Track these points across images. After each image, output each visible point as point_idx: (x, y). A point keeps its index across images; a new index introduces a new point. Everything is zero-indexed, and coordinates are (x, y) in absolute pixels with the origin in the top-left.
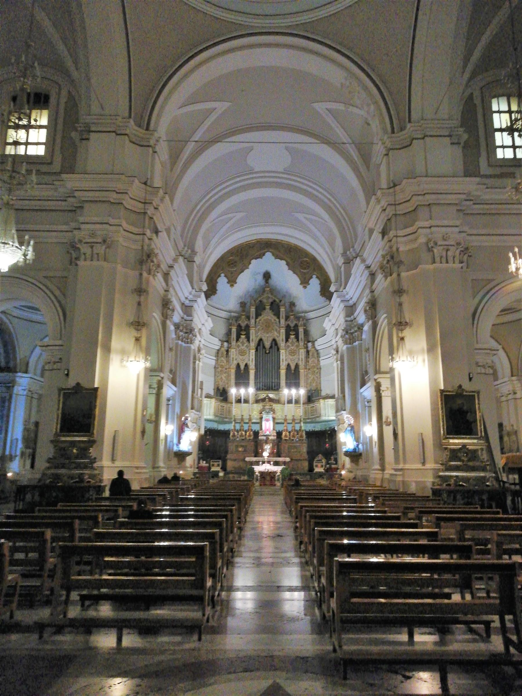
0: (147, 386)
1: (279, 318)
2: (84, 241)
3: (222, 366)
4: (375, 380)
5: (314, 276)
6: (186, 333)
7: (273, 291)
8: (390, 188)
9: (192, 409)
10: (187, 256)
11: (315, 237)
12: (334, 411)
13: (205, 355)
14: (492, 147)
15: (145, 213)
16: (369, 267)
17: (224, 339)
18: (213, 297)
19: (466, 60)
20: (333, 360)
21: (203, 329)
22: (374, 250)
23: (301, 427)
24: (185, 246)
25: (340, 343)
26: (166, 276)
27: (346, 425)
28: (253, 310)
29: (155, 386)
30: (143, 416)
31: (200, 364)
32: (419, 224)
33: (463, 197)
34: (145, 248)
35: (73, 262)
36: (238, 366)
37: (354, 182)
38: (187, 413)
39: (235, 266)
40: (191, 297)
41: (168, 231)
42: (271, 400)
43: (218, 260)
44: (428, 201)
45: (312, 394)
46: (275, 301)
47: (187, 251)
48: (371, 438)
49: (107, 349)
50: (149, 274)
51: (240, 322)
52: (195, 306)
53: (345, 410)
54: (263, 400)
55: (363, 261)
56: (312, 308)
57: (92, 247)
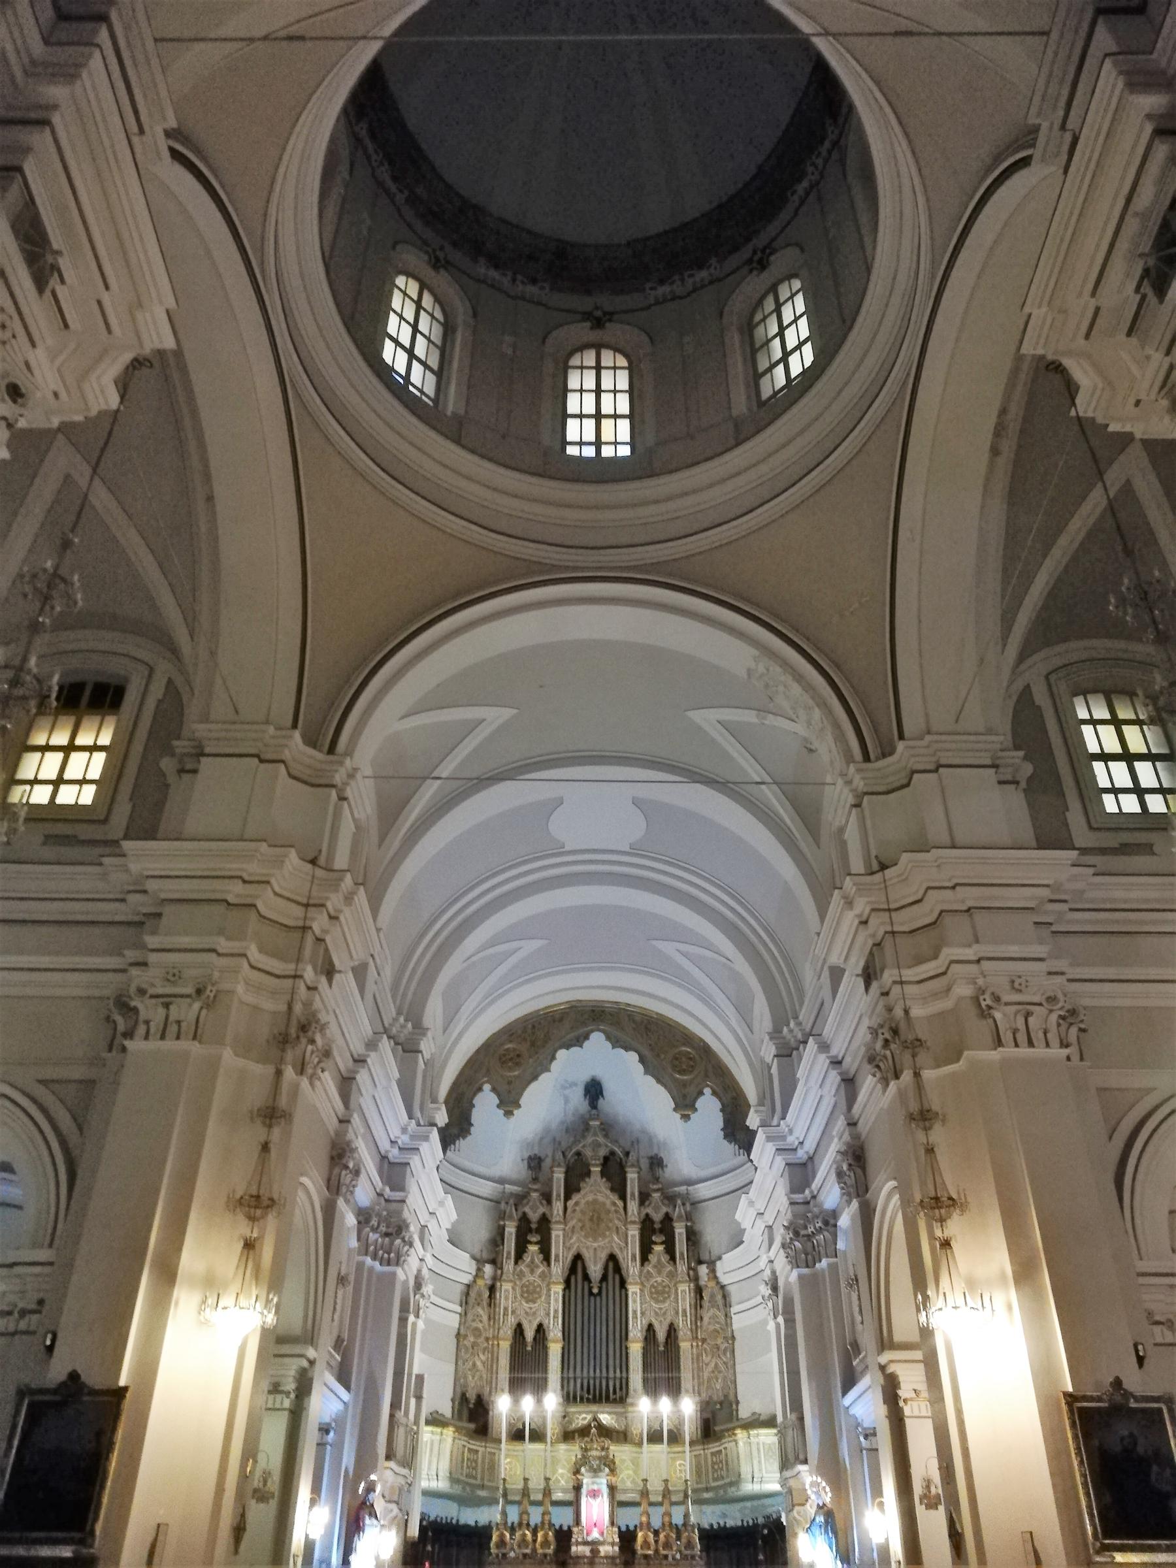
0: (265, 1385)
1: (623, 1197)
2: (151, 991)
3: (477, 1332)
4: (882, 1368)
5: (707, 1091)
6: (387, 1235)
7: (607, 1128)
8: (873, 873)
9: (388, 1457)
10: (402, 1038)
11: (705, 999)
12: (775, 1465)
13: (434, 1299)
14: (1090, 793)
15: (305, 929)
16: (840, 1063)
17: (485, 1256)
18: (462, 1143)
19: (1007, 621)
20: (763, 1313)
21: (432, 1225)
22: (849, 1020)
23: (686, 1516)
24: (399, 1013)
25: (781, 1263)
26: (346, 1084)
27: (811, 1509)
28: (559, 1176)
29: (290, 1386)
30: (244, 1477)
31: (418, 1325)
32: (948, 953)
33: (1045, 893)
34: (298, 1008)
35: (115, 1042)
36: (519, 1330)
37: (787, 869)
38: (373, 1468)
39: (518, 1064)
40: (404, 1139)
41: (360, 973)
42: (605, 1432)
43: (478, 1052)
44: (963, 902)
45: (714, 1413)
46: (613, 1153)
47: (403, 1027)
48: (884, 1551)
49: (168, 1275)
50: (301, 1071)
51: (527, 1209)
52: (415, 1161)
53: (805, 1462)
54: (584, 1432)
55: (824, 1047)
56: (703, 1174)
57: (167, 1006)
